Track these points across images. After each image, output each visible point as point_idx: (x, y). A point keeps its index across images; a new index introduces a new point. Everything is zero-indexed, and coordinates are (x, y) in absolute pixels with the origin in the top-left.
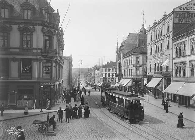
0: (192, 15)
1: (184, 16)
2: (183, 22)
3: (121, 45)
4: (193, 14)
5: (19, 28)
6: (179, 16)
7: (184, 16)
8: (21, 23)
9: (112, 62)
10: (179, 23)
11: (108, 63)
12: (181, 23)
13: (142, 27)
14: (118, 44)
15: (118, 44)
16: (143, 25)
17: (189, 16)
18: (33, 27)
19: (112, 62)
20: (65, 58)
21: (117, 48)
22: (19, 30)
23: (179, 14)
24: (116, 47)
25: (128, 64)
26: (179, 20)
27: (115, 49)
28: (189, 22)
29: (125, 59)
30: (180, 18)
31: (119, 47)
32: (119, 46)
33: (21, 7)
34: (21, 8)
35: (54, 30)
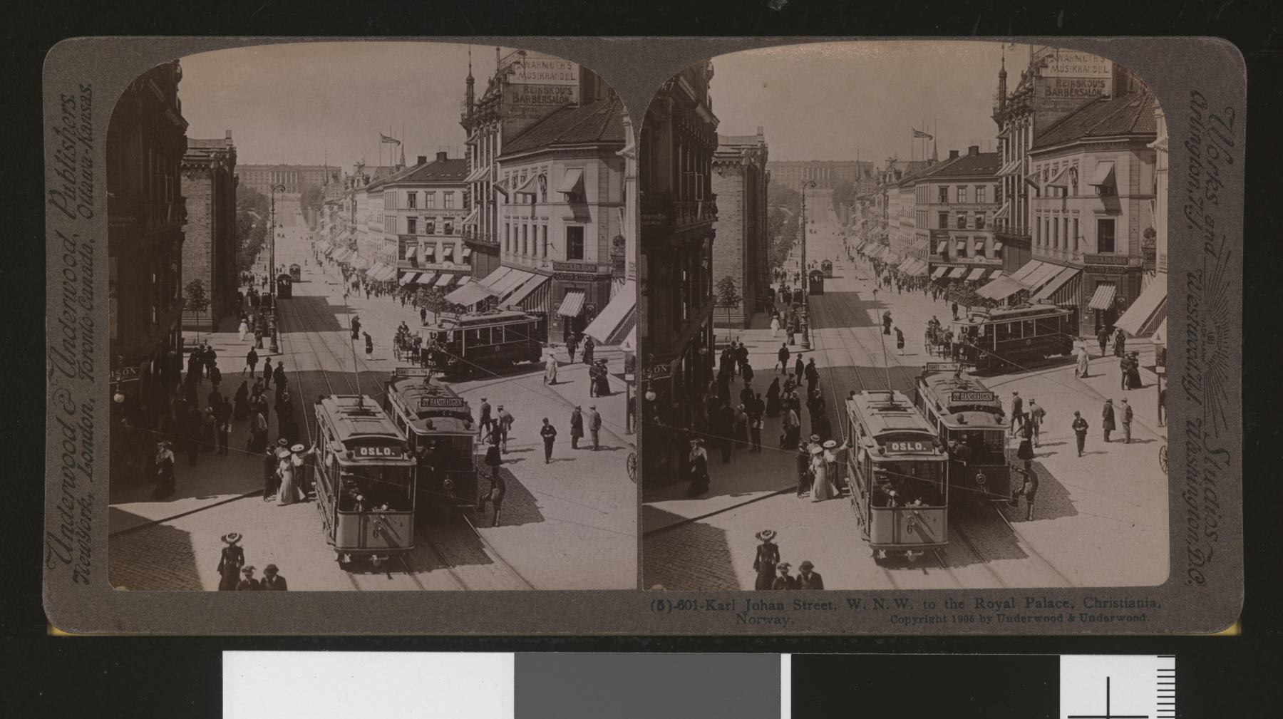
3: (1020, 79)
9: (974, 149)
11: (954, 154)
14: (471, 81)
19: (974, 149)
24: (464, 98)
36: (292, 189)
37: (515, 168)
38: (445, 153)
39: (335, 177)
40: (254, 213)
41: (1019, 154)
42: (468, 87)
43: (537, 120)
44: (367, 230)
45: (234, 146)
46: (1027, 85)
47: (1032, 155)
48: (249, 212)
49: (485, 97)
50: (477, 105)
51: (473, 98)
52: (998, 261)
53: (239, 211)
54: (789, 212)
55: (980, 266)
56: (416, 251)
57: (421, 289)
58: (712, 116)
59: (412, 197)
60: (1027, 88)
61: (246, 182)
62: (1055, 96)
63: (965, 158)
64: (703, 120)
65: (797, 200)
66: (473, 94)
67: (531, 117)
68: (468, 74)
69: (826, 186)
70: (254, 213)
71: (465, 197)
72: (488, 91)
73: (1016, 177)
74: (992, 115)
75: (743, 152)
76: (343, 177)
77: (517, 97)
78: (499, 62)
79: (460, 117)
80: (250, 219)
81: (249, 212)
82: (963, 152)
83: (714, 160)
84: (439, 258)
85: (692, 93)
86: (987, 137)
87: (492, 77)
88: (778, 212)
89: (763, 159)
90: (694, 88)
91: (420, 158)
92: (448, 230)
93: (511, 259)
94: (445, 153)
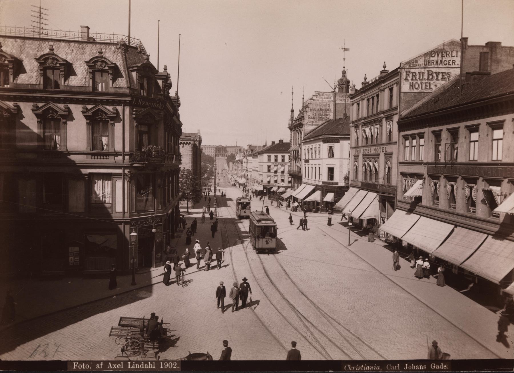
0: (437, 76)
1: (421, 78)
2: (420, 90)
3: (299, 113)
4: (439, 73)
5: (85, 112)
6: (411, 78)
7: (421, 78)
8: (89, 102)
9: (281, 141)
10: (412, 91)
11: (273, 143)
12: (415, 91)
13: (340, 76)
14: (292, 111)
15: (292, 111)
16: (344, 73)
17: (431, 77)
18: (114, 109)
19: (281, 141)
20: (186, 142)
21: (292, 119)
22: (84, 116)
23: (412, 73)
24: (290, 117)
25: (312, 155)
26: (412, 86)
27: (287, 122)
28: (430, 88)
29: (307, 146)
30: (414, 82)
31: (294, 119)
32: (296, 115)
33: (90, 66)
34: (86, 67)
35: (156, 111)
36: (223, 155)
37: (308, 145)
38: (282, 140)
39: (240, 150)
40: (208, 164)
41: (296, 143)
42: (292, 113)
43: (317, 126)
44: (252, 171)
45: (201, 136)
46: (301, 115)
47: (303, 142)
48: (207, 164)
49: (297, 117)
50: (295, 120)
51: (293, 117)
52: (290, 185)
53: (202, 164)
54: (210, 165)
55: (282, 187)
56: (270, 179)
57: (272, 193)
58: (180, 121)
59: (269, 157)
60: (302, 116)
61: (207, 152)
62: (312, 119)
63: (277, 144)
64: (176, 123)
65: (211, 160)
66: (293, 116)
67: (315, 125)
68: (291, 108)
69: (224, 156)
70: (208, 164)
71: (290, 157)
72: (299, 115)
73: (297, 151)
74: (288, 127)
75: (192, 139)
76: (242, 150)
77: (310, 117)
78: (303, 103)
79: (288, 125)
80: (207, 167)
81: (207, 164)
82: (277, 142)
83: (180, 141)
84: (279, 181)
85: (172, 110)
86: (286, 136)
87: (301, 109)
88: (205, 165)
89: (200, 142)
90: (173, 109)
91: (272, 142)
92: (276, 172)
93: (306, 181)
94: (282, 140)
